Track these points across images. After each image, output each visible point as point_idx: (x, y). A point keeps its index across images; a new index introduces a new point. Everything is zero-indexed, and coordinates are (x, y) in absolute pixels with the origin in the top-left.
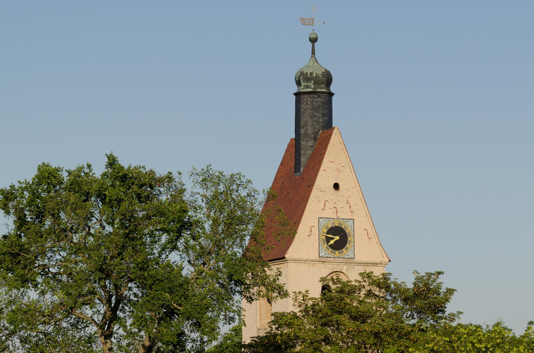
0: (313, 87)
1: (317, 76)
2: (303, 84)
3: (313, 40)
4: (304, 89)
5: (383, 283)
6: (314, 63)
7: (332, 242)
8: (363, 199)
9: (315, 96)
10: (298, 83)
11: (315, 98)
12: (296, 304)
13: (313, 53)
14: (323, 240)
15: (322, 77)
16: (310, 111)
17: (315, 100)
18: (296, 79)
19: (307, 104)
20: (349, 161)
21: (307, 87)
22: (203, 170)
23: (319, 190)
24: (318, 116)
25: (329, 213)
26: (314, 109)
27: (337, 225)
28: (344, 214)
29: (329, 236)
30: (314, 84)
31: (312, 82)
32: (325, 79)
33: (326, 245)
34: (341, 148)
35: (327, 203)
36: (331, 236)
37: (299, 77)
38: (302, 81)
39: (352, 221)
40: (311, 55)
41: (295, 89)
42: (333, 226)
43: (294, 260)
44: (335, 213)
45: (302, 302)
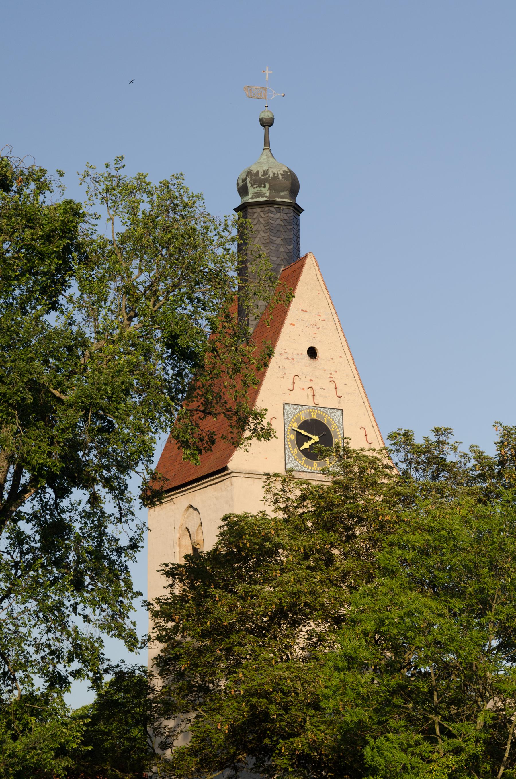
0: (268, 194)
1: (275, 177)
2: (251, 190)
3: (267, 123)
4: (252, 198)
5: (431, 457)
6: (268, 158)
7: (306, 445)
8: (357, 377)
9: (272, 209)
10: (243, 191)
11: (272, 212)
12: (269, 497)
13: (267, 143)
14: (291, 441)
15: (284, 178)
16: (263, 235)
17: (272, 216)
18: (238, 184)
19: (259, 223)
20: (333, 311)
21: (258, 195)
22: (107, 166)
23: (285, 356)
24: (277, 242)
25: (300, 397)
26: (270, 230)
27: (314, 417)
28: (326, 399)
29: (303, 432)
30: (270, 189)
31: (267, 186)
32: (288, 183)
33: (296, 450)
34: (319, 289)
35: (297, 379)
36: (306, 433)
37: (245, 179)
38: (249, 185)
39: (339, 412)
40: (264, 148)
41: (238, 201)
42: (308, 418)
43: (244, 474)
44: (311, 397)
45: (281, 493)
